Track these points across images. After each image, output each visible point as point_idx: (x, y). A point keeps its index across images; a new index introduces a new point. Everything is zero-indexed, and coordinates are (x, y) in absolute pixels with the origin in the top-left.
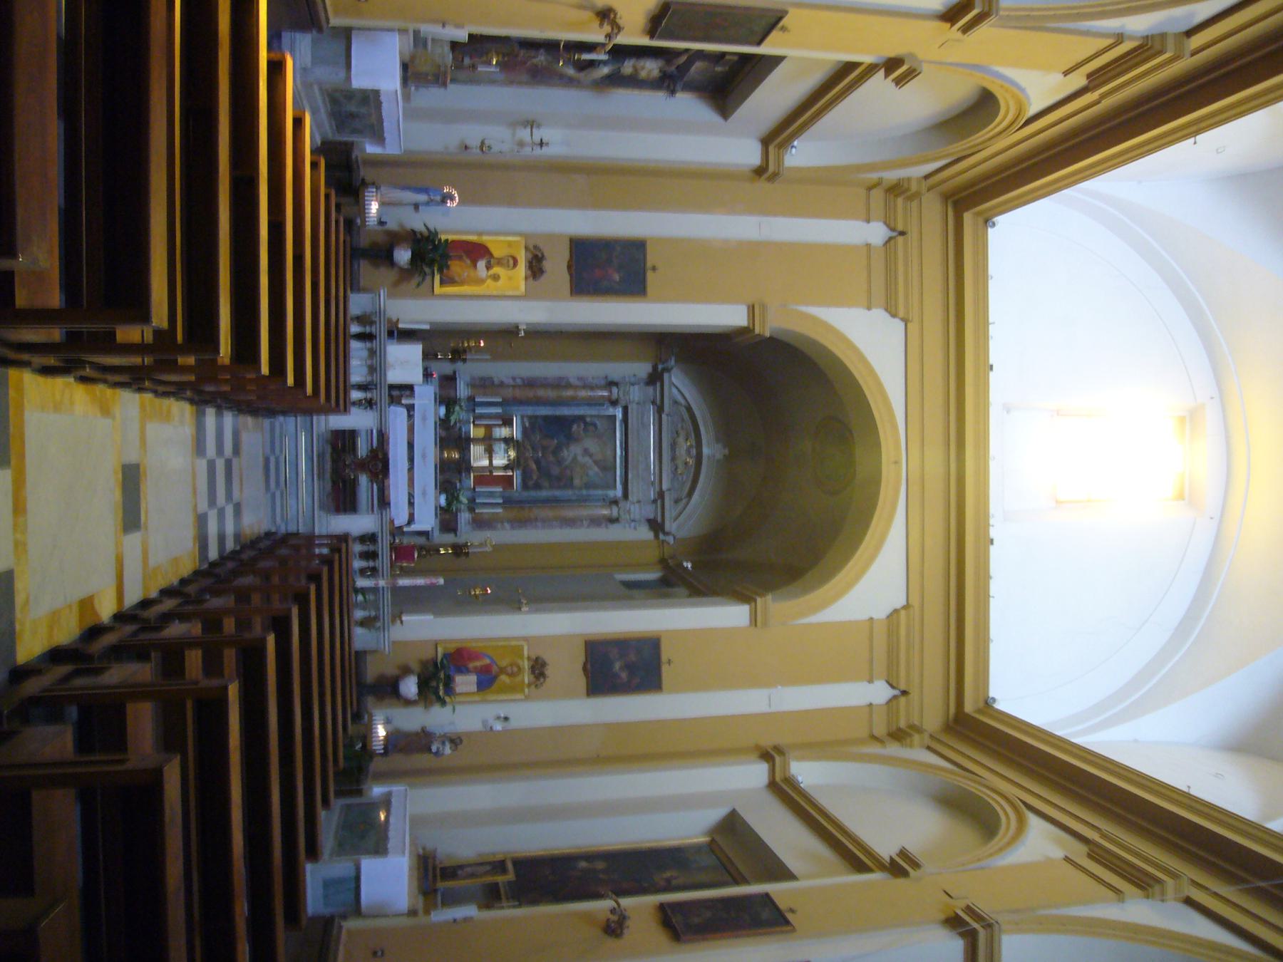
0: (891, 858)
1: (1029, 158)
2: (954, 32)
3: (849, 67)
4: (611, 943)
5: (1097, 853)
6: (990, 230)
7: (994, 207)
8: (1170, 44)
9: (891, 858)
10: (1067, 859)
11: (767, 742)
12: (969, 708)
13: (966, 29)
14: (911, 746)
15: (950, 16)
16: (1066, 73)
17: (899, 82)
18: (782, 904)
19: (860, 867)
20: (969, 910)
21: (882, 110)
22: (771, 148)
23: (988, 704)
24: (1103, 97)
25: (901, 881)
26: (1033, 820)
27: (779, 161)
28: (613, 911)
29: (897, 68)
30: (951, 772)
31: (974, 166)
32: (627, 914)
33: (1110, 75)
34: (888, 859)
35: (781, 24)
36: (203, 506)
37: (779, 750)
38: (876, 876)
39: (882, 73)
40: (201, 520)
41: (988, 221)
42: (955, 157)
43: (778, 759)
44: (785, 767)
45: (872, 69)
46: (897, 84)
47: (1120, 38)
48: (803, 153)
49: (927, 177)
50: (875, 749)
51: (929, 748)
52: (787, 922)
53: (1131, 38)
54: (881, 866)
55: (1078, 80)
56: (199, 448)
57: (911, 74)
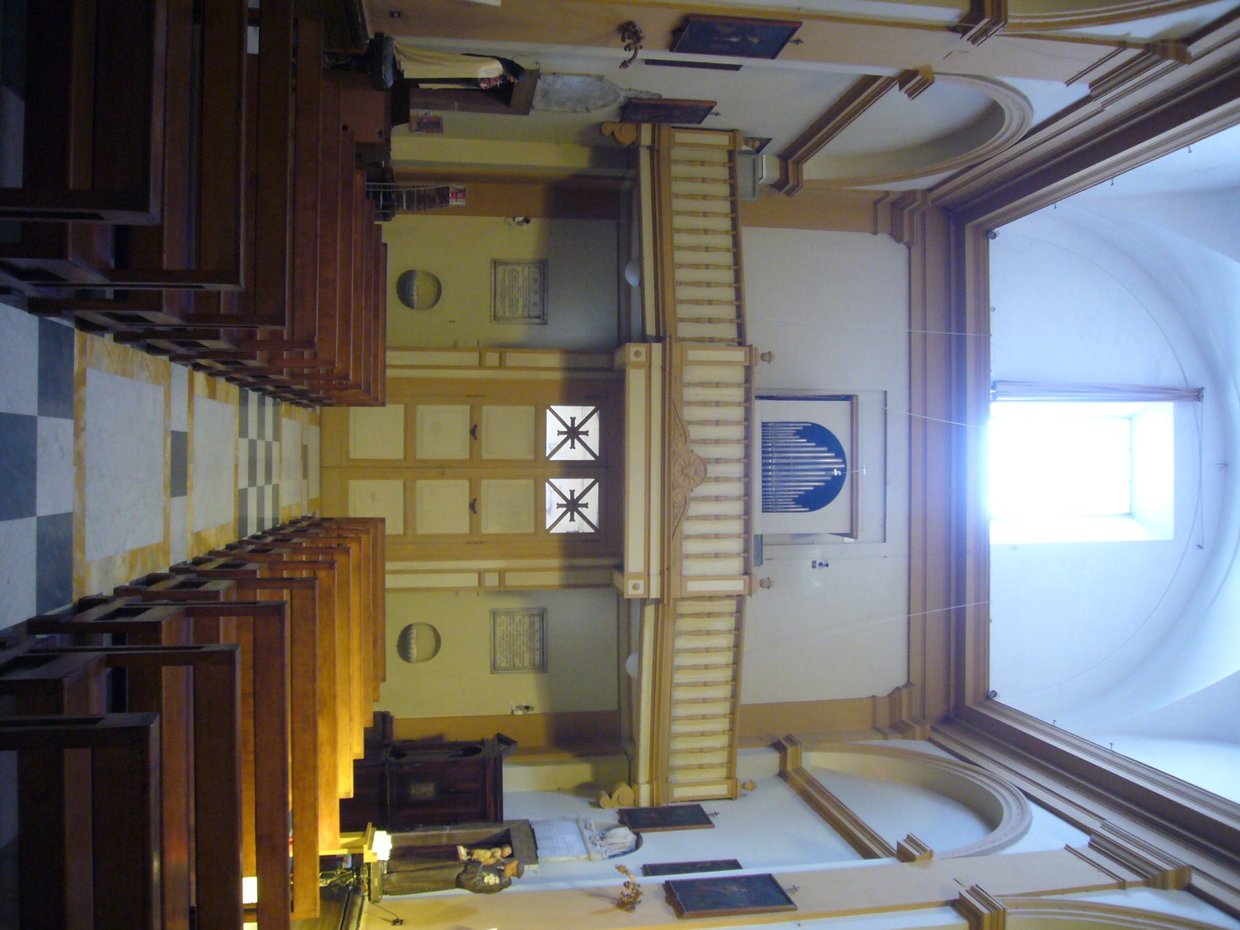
0: (899, 844)
1: (1053, 157)
2: (963, 43)
3: (869, 80)
4: (622, 913)
5: (1099, 843)
6: (991, 241)
7: (993, 219)
8: (919, 197)
9: (899, 844)
10: (1068, 848)
11: (780, 735)
12: (969, 701)
13: (974, 40)
14: (914, 739)
15: (960, 28)
16: (1069, 83)
17: (912, 94)
18: (784, 884)
19: (867, 854)
20: (975, 891)
21: (897, 119)
22: (790, 162)
23: (989, 697)
24: (1105, 105)
25: (906, 865)
26: (1034, 808)
27: (798, 172)
28: (626, 885)
29: (913, 81)
30: (949, 762)
31: (992, 169)
32: (641, 890)
33: (1140, 66)
34: (895, 847)
35: (795, 37)
36: (243, 483)
37: (789, 739)
38: (885, 861)
39: (897, 86)
40: (242, 496)
41: (988, 233)
42: (963, 167)
43: (790, 750)
44: (798, 758)
45: (889, 82)
46: (910, 96)
47: (1122, 44)
48: (813, 169)
49: (930, 190)
50: (878, 742)
51: (930, 740)
52: (790, 902)
53: (1135, 46)
54: (888, 852)
55: (1081, 90)
56: (243, 432)
57: (926, 83)
